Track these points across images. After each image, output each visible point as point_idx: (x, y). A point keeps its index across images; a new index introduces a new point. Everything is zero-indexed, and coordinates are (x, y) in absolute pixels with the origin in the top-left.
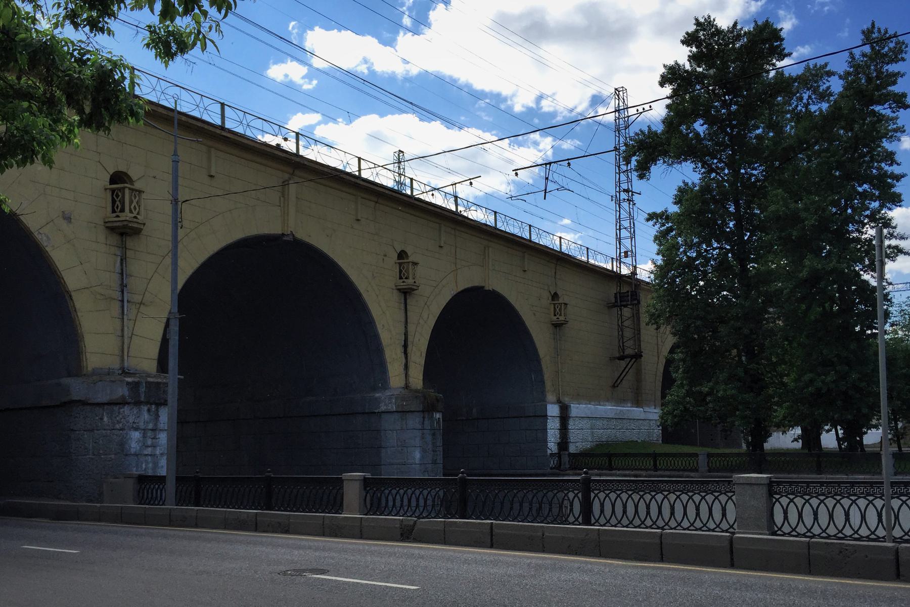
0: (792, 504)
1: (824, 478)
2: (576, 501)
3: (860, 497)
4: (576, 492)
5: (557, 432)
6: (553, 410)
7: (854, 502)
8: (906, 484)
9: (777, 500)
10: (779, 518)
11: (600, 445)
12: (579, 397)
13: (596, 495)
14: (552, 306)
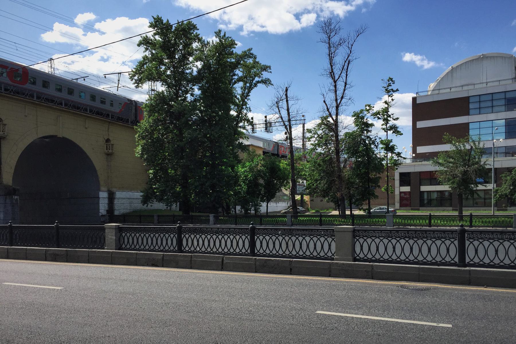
0: (471, 244)
1: (239, 227)
2: (174, 238)
3: (485, 240)
4: (246, 235)
5: (107, 206)
6: (103, 195)
7: (365, 240)
8: (513, 233)
9: (358, 240)
10: (358, 249)
11: (135, 211)
12: (122, 188)
13: (258, 237)
14: (105, 145)
